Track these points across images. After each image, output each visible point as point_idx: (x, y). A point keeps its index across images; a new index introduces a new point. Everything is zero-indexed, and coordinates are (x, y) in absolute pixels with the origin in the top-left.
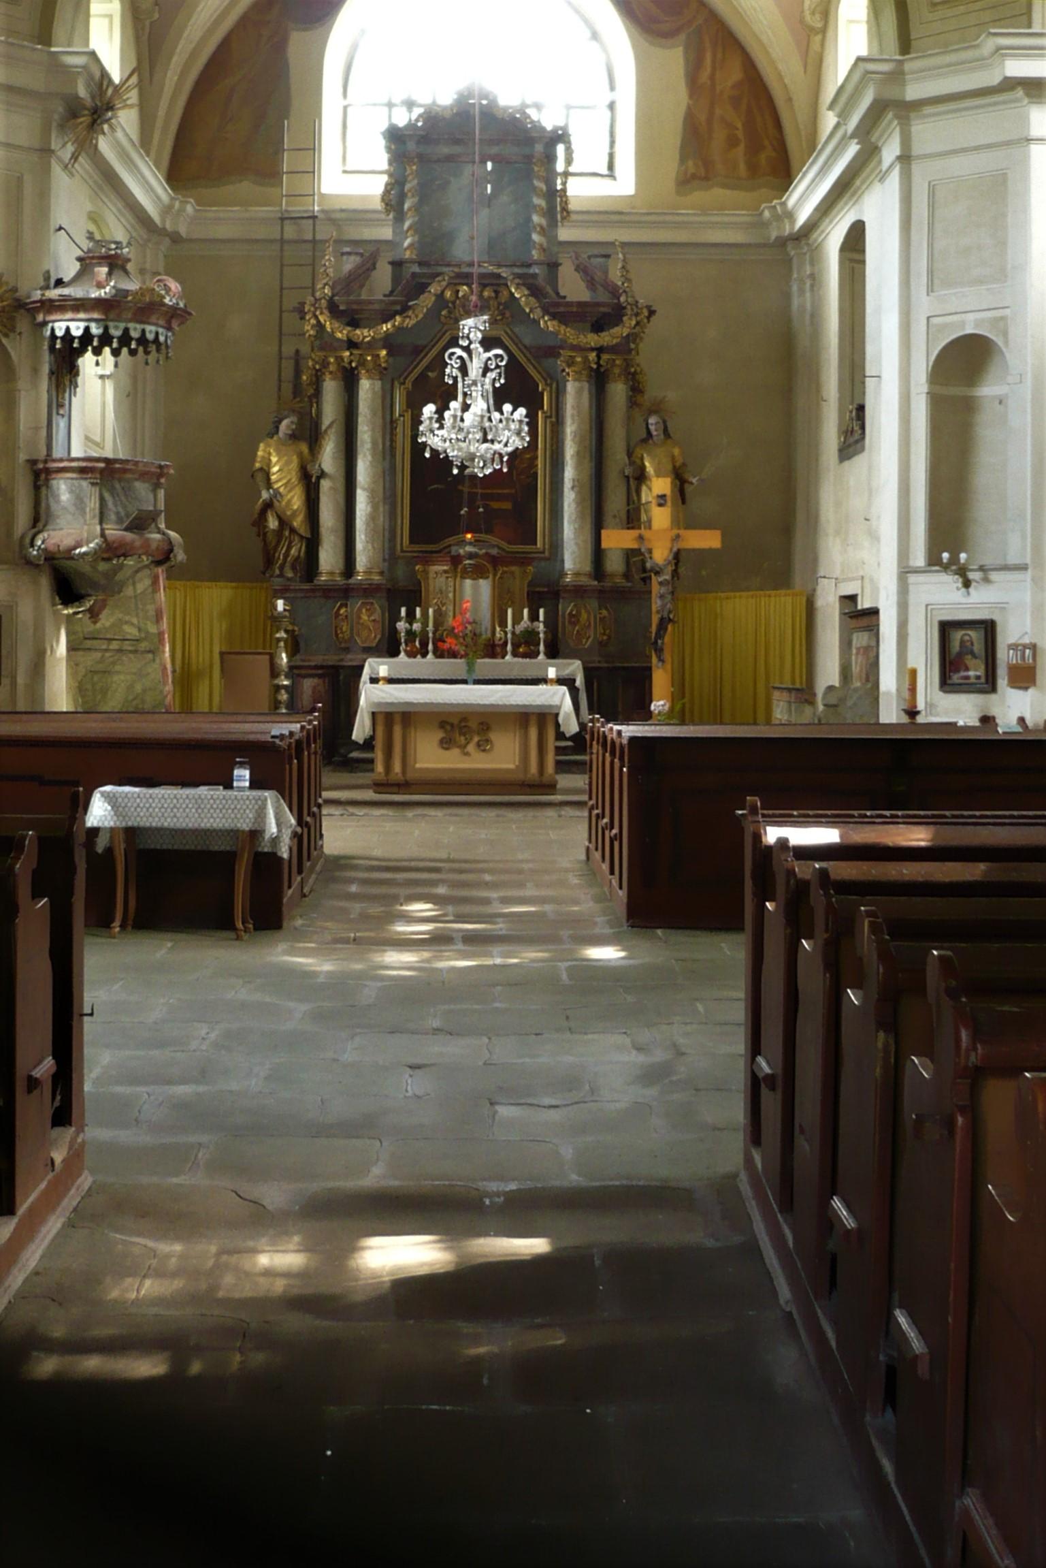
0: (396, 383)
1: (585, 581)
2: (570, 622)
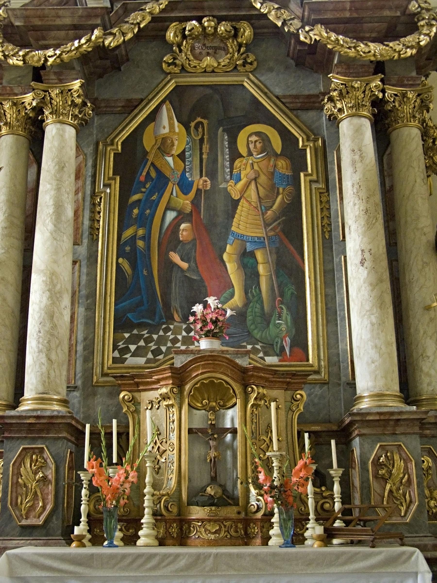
1: (395, 405)
2: (376, 476)
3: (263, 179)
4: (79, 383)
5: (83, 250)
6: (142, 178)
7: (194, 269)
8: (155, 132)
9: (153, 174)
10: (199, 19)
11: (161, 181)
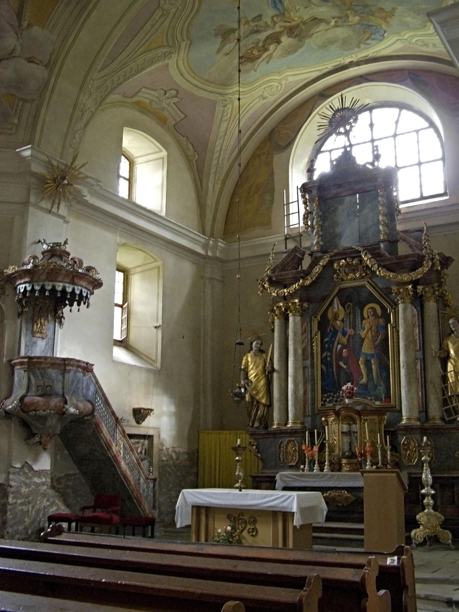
0: (313, 318)
3: (374, 328)
4: (310, 414)
5: (308, 362)
6: (328, 331)
7: (348, 368)
8: (332, 311)
9: (332, 329)
10: (345, 259)
11: (335, 332)
